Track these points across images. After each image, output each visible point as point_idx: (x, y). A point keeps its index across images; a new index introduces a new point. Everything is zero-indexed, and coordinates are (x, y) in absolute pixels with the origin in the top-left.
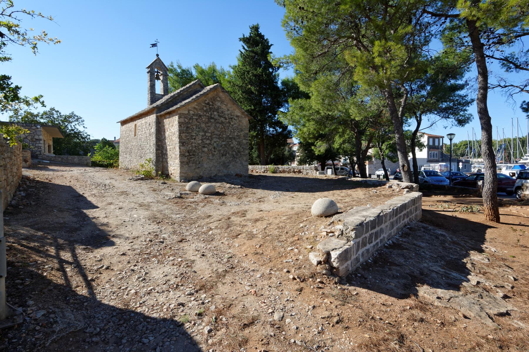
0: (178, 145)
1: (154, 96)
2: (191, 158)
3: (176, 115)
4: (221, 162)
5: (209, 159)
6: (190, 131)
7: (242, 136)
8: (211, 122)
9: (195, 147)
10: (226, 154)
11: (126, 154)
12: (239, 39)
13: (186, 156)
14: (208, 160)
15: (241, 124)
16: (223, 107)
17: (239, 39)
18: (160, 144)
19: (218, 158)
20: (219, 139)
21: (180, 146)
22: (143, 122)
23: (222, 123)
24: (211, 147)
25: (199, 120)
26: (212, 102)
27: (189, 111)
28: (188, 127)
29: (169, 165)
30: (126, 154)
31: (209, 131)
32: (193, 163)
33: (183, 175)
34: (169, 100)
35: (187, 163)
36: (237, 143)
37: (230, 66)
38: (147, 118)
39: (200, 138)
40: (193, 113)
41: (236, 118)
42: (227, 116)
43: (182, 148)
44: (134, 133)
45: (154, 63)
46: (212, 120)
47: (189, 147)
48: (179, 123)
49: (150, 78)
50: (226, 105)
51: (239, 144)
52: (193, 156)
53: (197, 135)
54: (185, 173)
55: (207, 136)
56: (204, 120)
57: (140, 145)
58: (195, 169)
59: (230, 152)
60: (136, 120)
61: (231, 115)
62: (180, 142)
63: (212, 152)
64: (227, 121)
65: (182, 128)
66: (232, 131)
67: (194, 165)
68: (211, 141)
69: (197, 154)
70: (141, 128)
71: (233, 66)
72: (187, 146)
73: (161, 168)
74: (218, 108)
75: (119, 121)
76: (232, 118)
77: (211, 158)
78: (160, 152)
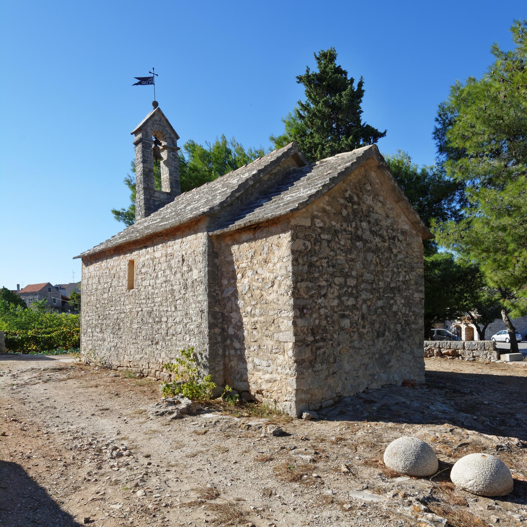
0: (291, 314)
1: (151, 196)
2: (319, 348)
3: (284, 231)
4: (375, 354)
5: (354, 348)
6: (316, 275)
7: (413, 282)
8: (356, 248)
9: (327, 317)
10: (385, 331)
11: (101, 331)
12: (298, 78)
13: (308, 346)
14: (351, 351)
15: (410, 252)
16: (378, 207)
17: (298, 78)
18: (217, 309)
19: (370, 343)
20: (372, 293)
21: (295, 317)
22: (158, 254)
23: (377, 251)
24: (356, 316)
25: (333, 244)
26: (358, 196)
27: (313, 218)
28: (311, 265)
29: (250, 366)
30: (101, 331)
31: (354, 273)
32: (322, 363)
33: (303, 396)
34: (237, 195)
35: (310, 362)
36: (403, 301)
37: (272, 139)
38: (170, 243)
39: (336, 294)
40: (321, 225)
41: (401, 237)
42: (385, 233)
43: (300, 322)
44: (125, 282)
45: (150, 122)
46: (359, 244)
47: (314, 320)
48: (293, 252)
49: (143, 156)
50: (383, 204)
51: (408, 303)
52: (321, 344)
53: (330, 285)
54: (306, 392)
55: (349, 287)
56: (342, 243)
57: (150, 313)
58: (326, 378)
59: (392, 327)
60: (131, 251)
61: (392, 230)
62: (295, 307)
63: (358, 330)
64: (386, 244)
65: (300, 268)
66: (395, 270)
67: (325, 366)
68: (356, 298)
69: (329, 336)
70: (150, 270)
71: (280, 138)
72: (311, 315)
73: (221, 373)
74: (369, 212)
75: (79, 254)
76: (394, 238)
77: (356, 344)
78: (217, 330)
